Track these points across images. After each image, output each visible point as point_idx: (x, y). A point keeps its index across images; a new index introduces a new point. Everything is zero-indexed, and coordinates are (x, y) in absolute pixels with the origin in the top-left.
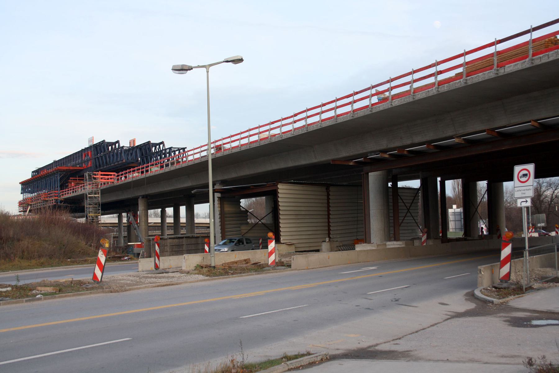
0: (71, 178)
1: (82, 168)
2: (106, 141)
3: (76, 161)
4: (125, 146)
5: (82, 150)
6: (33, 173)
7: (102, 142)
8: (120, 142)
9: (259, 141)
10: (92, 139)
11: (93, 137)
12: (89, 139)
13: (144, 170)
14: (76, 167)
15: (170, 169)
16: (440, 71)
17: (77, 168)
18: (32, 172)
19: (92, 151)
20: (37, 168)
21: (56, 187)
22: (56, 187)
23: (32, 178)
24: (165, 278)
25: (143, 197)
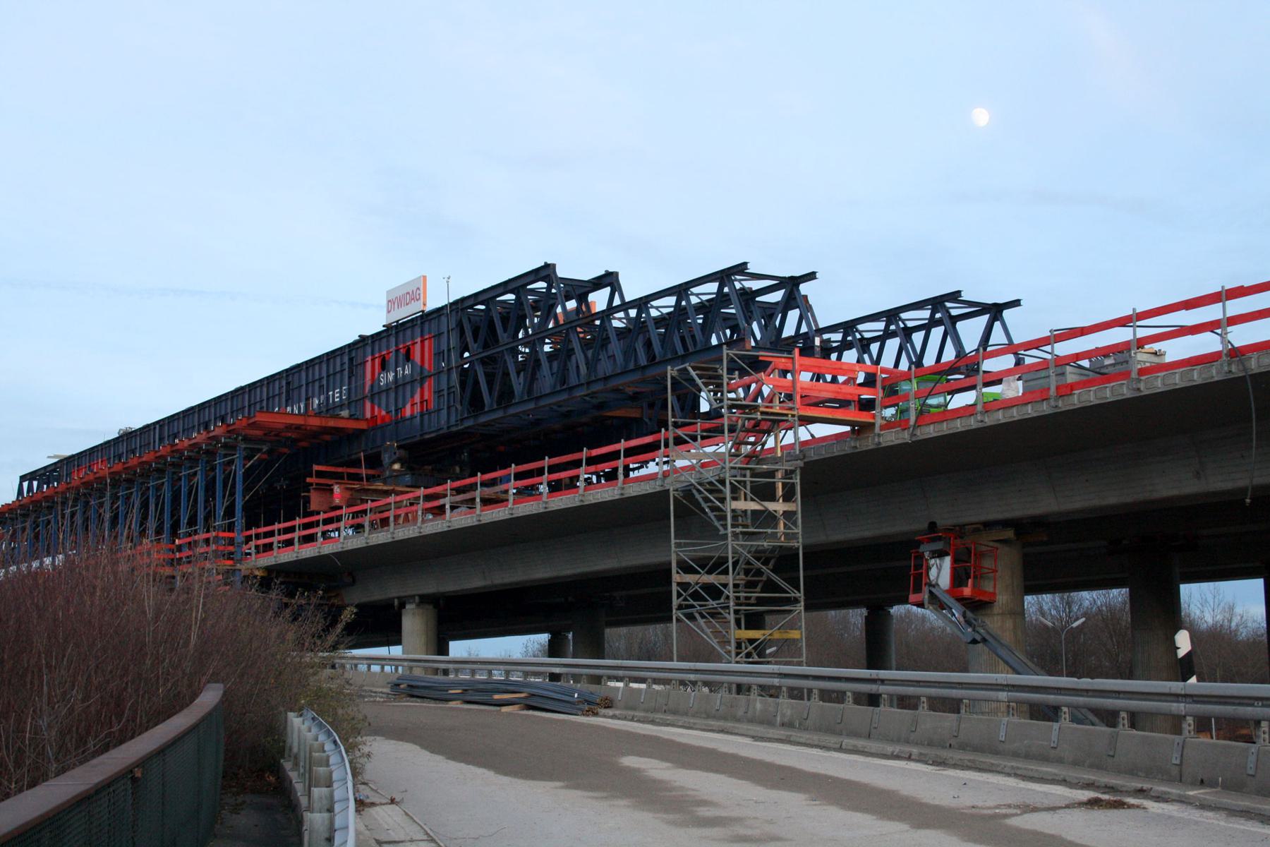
0: (316, 468)
1: (363, 426)
2: (561, 273)
3: (307, 399)
4: (752, 269)
5: (363, 339)
6: (25, 484)
7: (42, 472)
8: (623, 280)
9: (659, 476)
10: (415, 291)
11: (425, 277)
12: (388, 292)
13: (391, 514)
14: (337, 417)
15: (319, 552)
16: (1187, 310)
17: (341, 424)
18: (23, 478)
19: (110, 458)
20: (55, 457)
21: (184, 520)
22: (184, 520)
23: (17, 504)
24: (1264, 815)
25: (425, 600)
